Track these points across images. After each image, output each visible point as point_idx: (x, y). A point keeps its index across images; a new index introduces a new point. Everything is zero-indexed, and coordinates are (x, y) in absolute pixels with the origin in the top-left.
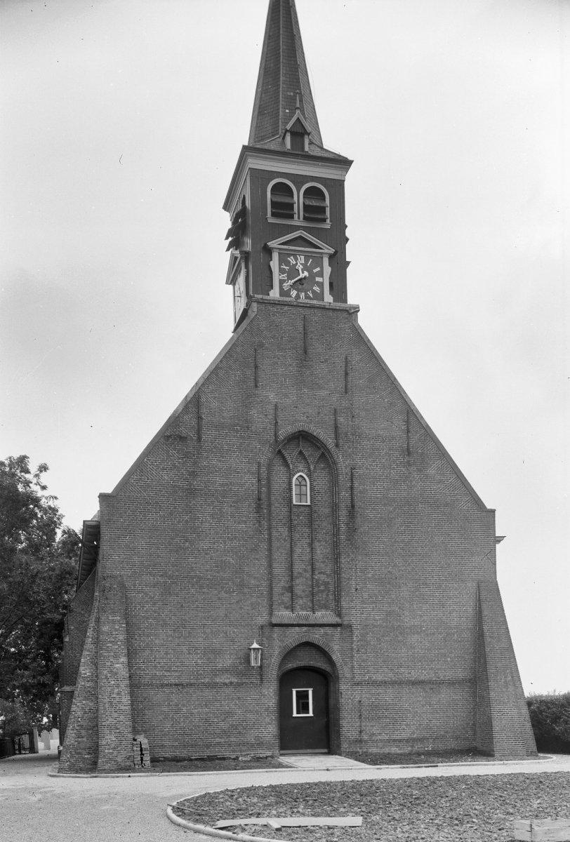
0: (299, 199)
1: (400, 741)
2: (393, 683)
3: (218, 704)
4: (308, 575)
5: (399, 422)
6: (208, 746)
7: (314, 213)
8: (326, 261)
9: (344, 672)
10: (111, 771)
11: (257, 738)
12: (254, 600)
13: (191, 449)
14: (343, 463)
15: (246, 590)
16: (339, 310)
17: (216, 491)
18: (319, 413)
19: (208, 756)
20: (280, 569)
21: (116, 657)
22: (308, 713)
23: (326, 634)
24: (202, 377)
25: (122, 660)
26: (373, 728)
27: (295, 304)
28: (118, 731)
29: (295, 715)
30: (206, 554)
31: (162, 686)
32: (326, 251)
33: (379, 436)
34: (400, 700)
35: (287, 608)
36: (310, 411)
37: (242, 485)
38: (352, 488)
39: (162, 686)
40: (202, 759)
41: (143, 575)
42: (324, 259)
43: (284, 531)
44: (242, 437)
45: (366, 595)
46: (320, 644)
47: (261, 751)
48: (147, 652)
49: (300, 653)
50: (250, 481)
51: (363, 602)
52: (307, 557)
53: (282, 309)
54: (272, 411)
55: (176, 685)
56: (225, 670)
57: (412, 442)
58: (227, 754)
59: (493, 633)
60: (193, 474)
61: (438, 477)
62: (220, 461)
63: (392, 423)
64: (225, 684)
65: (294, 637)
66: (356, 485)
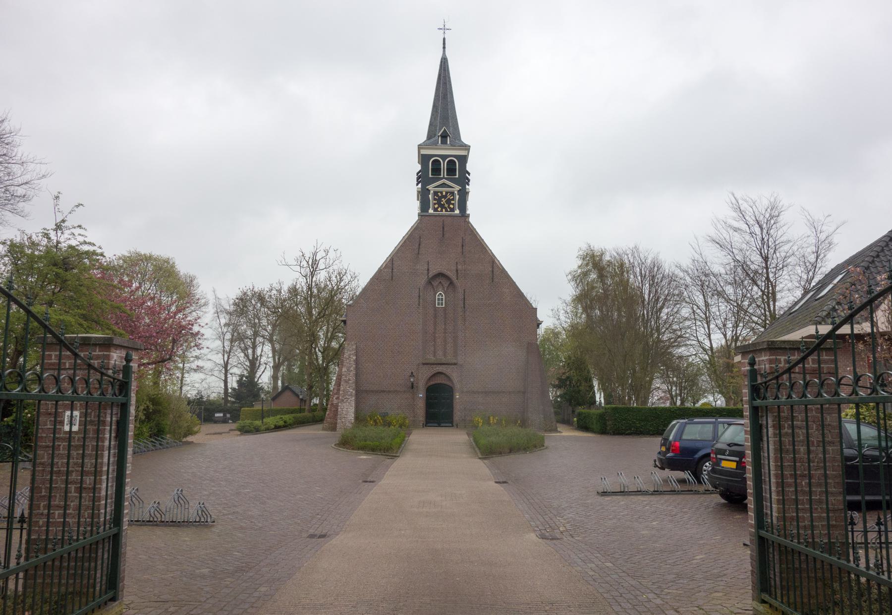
0: (444, 166)
7: (451, 170)
9: (457, 386)
29: (430, 176)
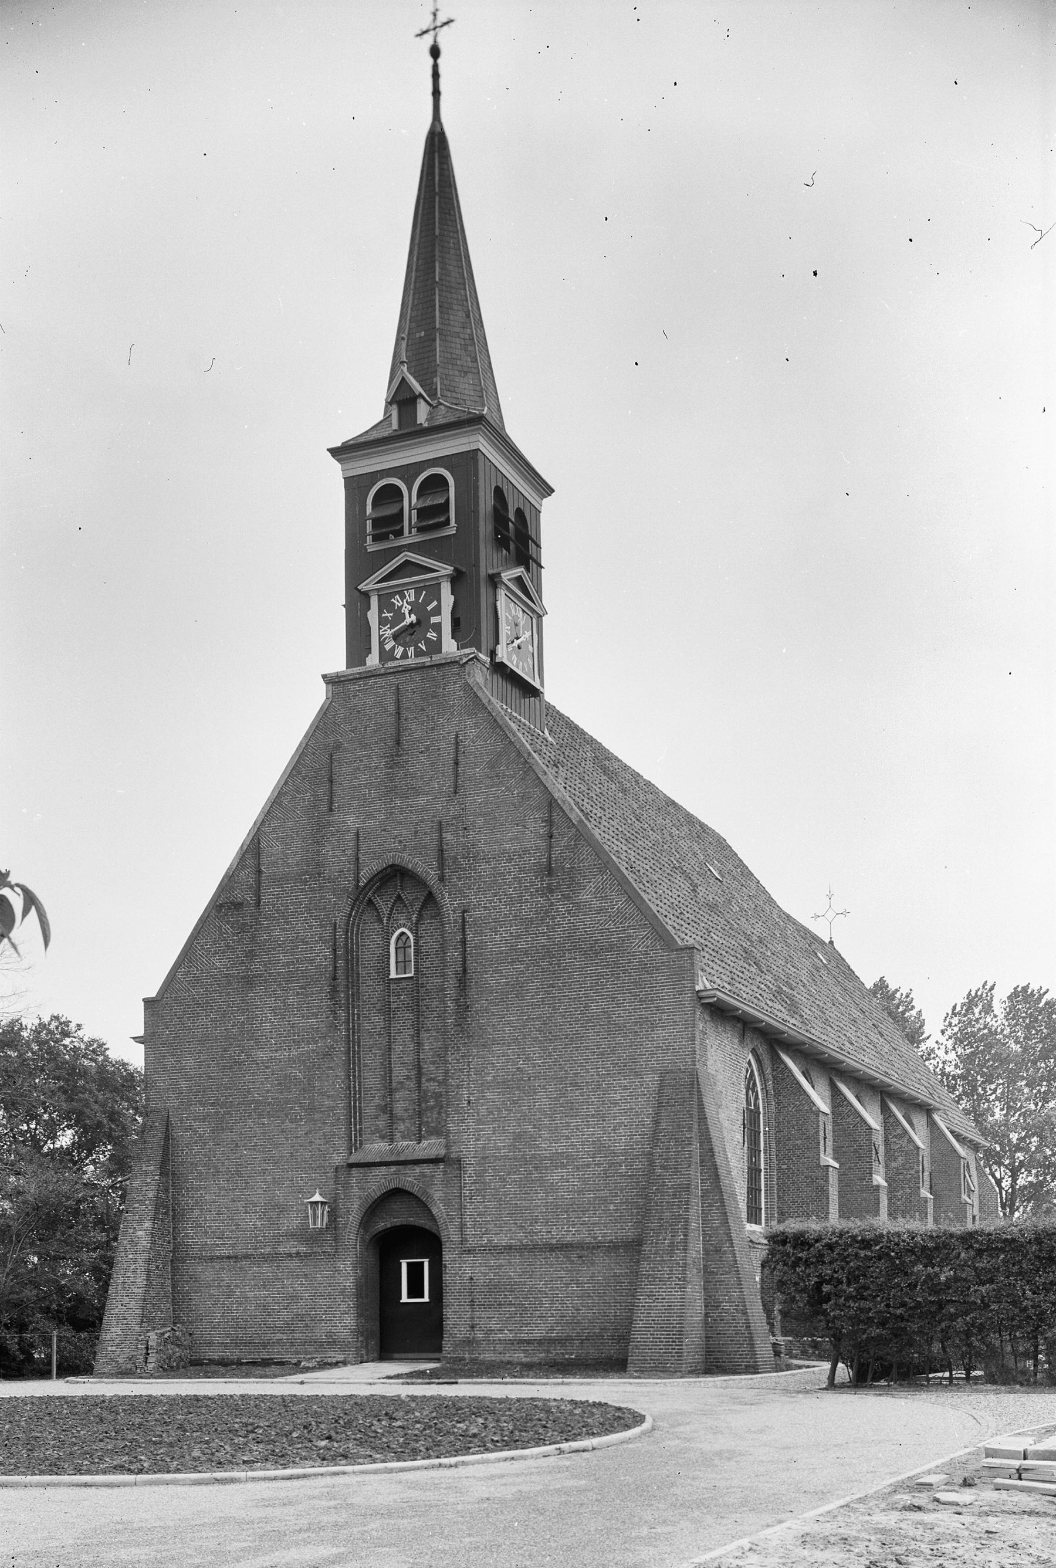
0: (410, 500)
1: (529, 1342)
2: (521, 1249)
3: (278, 1284)
4: (412, 1084)
5: (535, 826)
6: (265, 1345)
8: (446, 589)
9: (450, 1234)
10: (111, 1375)
11: (329, 1334)
12: (327, 1129)
13: (248, 920)
14: (449, 903)
15: (317, 1116)
16: (446, 664)
17: (279, 974)
18: (416, 832)
19: (262, 1359)
20: (372, 1079)
21: (140, 1222)
22: (423, 1297)
23: (423, 1175)
24: (262, 811)
25: (146, 1225)
26: (491, 1321)
27: (383, 671)
28: (125, 1321)
30: (267, 1068)
31: (212, 1259)
32: (443, 572)
33: (505, 851)
34: (531, 1276)
35: (383, 1137)
36: (404, 832)
37: (311, 961)
38: (464, 942)
39: (212, 1259)
40: (254, 1363)
41: (191, 1105)
42: (443, 585)
43: (378, 1020)
44: (312, 890)
45: (483, 1110)
46: (415, 1190)
47: (332, 1354)
48: (196, 1213)
49: (396, 1205)
50: (322, 953)
51: (479, 1122)
52: (409, 1058)
53: (365, 685)
54: (352, 844)
55: (229, 1257)
56: (290, 1235)
57: (556, 852)
58: (287, 1357)
59: (666, 1160)
60: (251, 955)
61: (596, 904)
62: (284, 930)
63: (524, 826)
64: (290, 1255)
65: (379, 1181)
66: (470, 936)
